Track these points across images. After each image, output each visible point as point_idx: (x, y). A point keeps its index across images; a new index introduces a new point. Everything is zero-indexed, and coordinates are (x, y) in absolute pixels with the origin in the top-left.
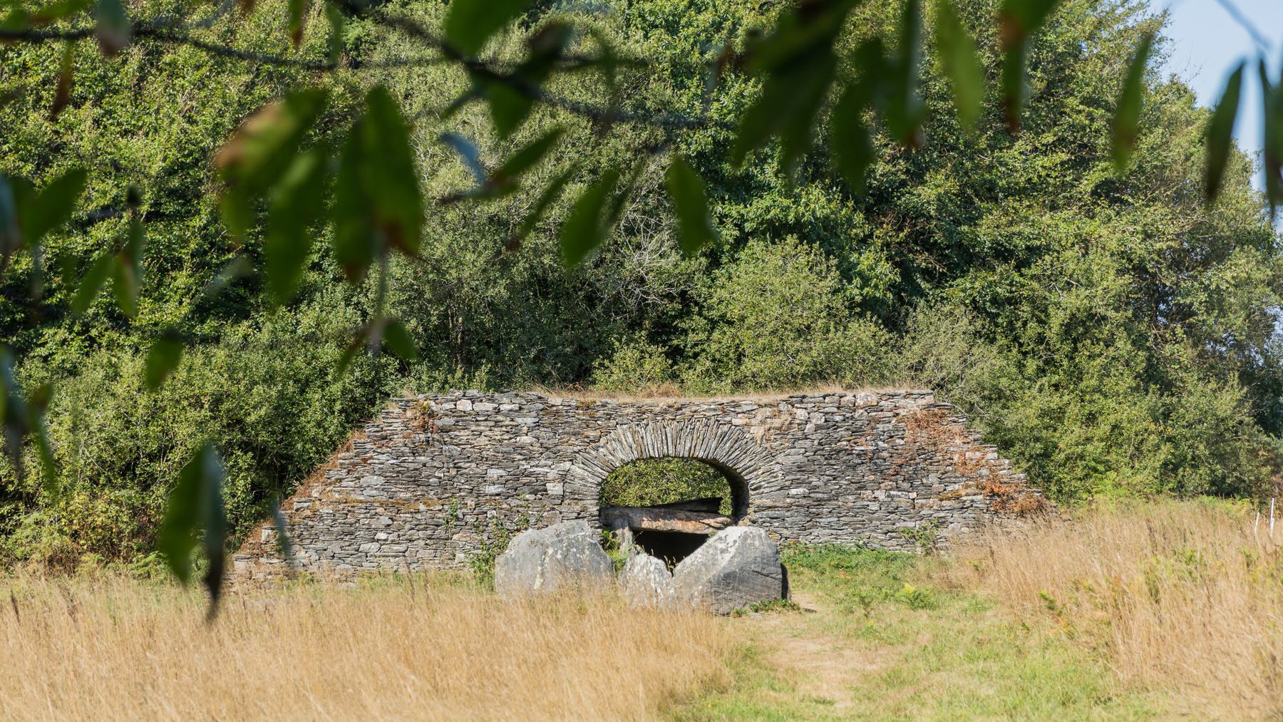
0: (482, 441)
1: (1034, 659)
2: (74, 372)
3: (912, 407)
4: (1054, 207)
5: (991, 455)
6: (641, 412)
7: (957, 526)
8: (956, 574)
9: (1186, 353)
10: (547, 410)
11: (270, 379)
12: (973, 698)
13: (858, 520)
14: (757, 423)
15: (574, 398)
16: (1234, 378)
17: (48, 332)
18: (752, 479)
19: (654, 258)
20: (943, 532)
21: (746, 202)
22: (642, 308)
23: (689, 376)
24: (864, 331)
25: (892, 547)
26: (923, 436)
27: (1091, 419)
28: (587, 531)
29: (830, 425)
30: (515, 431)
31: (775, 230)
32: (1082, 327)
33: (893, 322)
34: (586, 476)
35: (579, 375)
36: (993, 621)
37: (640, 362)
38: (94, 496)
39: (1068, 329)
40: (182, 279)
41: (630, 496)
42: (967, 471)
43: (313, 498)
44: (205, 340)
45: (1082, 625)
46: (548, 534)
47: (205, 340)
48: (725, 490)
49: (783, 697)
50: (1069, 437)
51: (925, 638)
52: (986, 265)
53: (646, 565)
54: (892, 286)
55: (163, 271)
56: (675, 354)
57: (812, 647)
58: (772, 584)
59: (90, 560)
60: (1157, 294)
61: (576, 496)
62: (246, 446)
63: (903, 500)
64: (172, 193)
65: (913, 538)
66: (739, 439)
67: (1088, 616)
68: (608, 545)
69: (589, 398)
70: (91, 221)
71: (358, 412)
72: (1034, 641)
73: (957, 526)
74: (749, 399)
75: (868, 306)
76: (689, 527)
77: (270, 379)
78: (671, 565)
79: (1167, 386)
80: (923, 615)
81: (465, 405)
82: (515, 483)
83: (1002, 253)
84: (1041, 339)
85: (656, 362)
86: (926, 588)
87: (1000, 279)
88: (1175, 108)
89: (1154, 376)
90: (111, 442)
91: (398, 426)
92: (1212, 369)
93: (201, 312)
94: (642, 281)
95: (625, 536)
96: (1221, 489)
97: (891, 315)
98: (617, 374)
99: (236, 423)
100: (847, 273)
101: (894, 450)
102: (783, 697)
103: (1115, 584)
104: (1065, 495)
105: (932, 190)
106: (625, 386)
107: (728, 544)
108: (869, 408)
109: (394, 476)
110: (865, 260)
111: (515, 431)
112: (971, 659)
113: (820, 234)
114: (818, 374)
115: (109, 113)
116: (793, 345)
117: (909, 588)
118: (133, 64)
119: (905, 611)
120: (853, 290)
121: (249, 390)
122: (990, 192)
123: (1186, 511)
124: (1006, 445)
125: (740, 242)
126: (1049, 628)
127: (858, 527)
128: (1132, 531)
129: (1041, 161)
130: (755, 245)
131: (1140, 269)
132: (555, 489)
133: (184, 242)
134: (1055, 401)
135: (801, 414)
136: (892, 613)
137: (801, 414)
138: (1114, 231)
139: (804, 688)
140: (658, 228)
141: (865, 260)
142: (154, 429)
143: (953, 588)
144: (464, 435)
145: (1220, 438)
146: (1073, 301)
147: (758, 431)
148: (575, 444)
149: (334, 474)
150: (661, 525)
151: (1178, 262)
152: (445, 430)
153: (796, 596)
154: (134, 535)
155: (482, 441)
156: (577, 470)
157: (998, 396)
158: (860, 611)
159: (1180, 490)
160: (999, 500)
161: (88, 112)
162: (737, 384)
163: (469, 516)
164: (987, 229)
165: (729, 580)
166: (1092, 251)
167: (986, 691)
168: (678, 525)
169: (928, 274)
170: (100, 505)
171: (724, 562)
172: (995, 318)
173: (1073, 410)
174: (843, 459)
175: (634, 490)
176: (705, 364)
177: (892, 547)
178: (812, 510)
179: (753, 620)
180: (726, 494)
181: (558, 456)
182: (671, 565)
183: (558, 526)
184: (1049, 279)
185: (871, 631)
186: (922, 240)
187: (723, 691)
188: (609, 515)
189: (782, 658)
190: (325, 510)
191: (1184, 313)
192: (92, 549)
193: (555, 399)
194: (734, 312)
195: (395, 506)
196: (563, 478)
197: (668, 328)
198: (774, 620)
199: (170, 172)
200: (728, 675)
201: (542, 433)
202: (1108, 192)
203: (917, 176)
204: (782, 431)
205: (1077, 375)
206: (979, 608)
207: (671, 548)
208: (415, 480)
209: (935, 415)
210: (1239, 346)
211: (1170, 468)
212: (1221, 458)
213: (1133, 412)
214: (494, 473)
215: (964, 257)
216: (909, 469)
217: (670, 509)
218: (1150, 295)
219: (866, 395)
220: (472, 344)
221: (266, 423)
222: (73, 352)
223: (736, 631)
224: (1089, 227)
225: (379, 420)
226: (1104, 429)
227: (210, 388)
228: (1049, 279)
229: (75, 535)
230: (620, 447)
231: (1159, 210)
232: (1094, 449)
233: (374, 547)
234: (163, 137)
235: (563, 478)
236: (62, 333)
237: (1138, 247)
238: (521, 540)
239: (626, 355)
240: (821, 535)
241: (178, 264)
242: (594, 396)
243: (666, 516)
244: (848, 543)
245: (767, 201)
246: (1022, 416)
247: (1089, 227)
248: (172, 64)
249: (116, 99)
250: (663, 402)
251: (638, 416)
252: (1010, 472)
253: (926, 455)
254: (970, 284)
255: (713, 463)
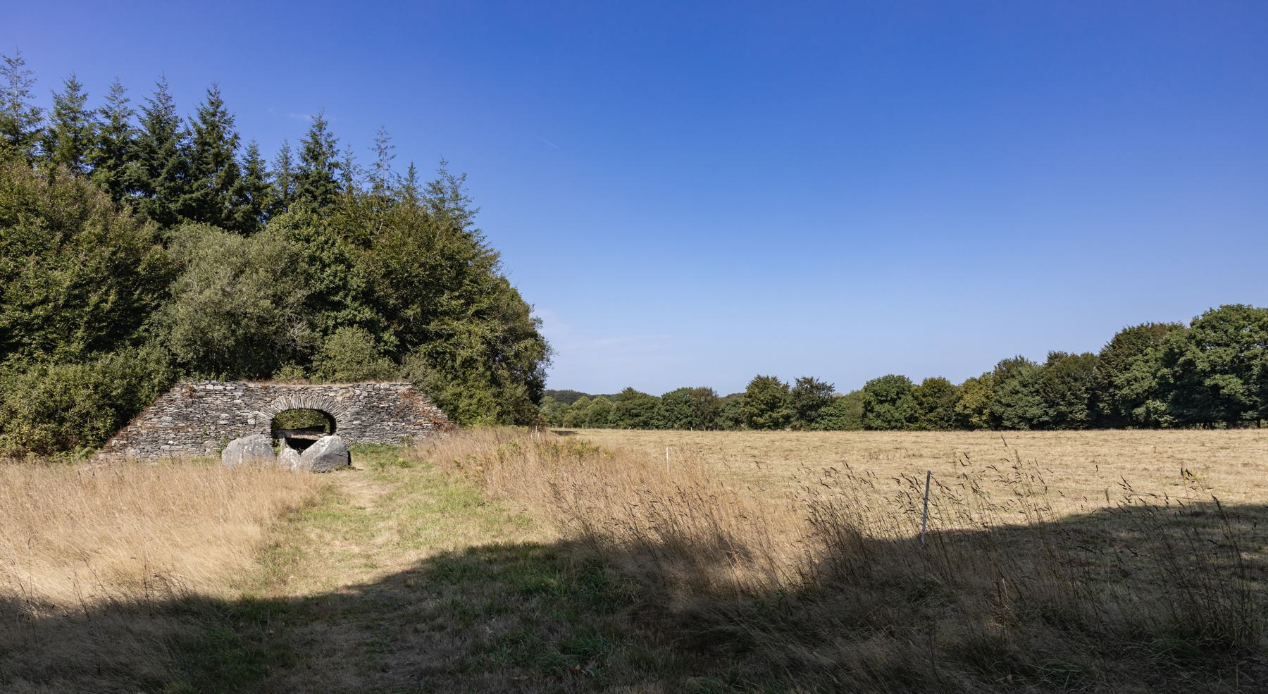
0: (218, 402)
1: (452, 487)
2: (24, 372)
3: (403, 389)
4: (458, 320)
5: (434, 408)
6: (290, 390)
7: (421, 435)
8: (420, 454)
9: (506, 373)
10: (248, 389)
11: (123, 377)
12: (427, 505)
13: (382, 434)
14: (337, 395)
15: (259, 385)
16: (522, 383)
17: (11, 355)
18: (337, 418)
19: (299, 332)
20: (416, 438)
21: (339, 311)
22: (294, 350)
23: (313, 378)
24: (384, 363)
25: (395, 444)
26: (407, 401)
27: (471, 397)
28: (266, 440)
29: (369, 396)
30: (233, 398)
31: (351, 323)
32: (469, 363)
33: (397, 361)
34: (266, 417)
35: (268, 377)
36: (435, 471)
37: (292, 373)
38: (34, 427)
39: (463, 364)
40: (80, 333)
41: (288, 425)
42: (425, 415)
43: (139, 425)
44: (91, 360)
45: (471, 473)
46: (246, 440)
47: (91, 360)
48: (325, 422)
49: (342, 507)
50: (463, 404)
51: (407, 480)
52: (432, 339)
53: (288, 452)
54: (396, 346)
55: (70, 330)
56: (307, 370)
57: (359, 485)
58: (344, 459)
59: (31, 454)
60: (495, 352)
61: (261, 425)
62: (111, 406)
63: (400, 425)
64: (76, 297)
65: (403, 440)
66: (332, 402)
67: (474, 468)
68: (275, 445)
69: (267, 385)
70: (34, 305)
71: (164, 389)
72: (451, 480)
73: (421, 435)
74: (336, 386)
75: (387, 353)
76: (311, 437)
77: (123, 377)
78: (300, 453)
79: (499, 385)
80: (406, 470)
81: (210, 387)
82: (233, 420)
83: (439, 335)
84: (453, 367)
85: (299, 372)
86: (407, 459)
87: (439, 345)
88: (504, 286)
89: (495, 381)
90: (43, 403)
91: (178, 395)
92: (515, 380)
93: (89, 348)
94: (294, 341)
95: (282, 441)
96: (518, 423)
97: (396, 357)
98: (283, 377)
99: (106, 395)
100: (378, 340)
101: (396, 407)
102: (342, 507)
103: (485, 455)
104: (463, 425)
105: (411, 312)
106: (287, 381)
107: (324, 443)
108: (386, 390)
109: (177, 417)
110: (386, 336)
111: (233, 398)
112: (426, 487)
113: (370, 326)
114: (365, 378)
115: (44, 260)
116: (355, 366)
117: (401, 459)
118: (57, 239)
119: (399, 469)
120: (382, 347)
121: (112, 382)
122: (435, 314)
123: (508, 429)
124: (440, 407)
125: (335, 327)
126: (458, 474)
127: (381, 437)
128: (490, 435)
129: (453, 302)
130: (340, 329)
131: (489, 343)
132: (251, 422)
133: (81, 317)
134: (458, 390)
135: (358, 392)
136: (394, 470)
137: (358, 392)
138: (481, 329)
139: (353, 502)
140: (301, 320)
141: (386, 336)
142: (66, 398)
143: (419, 460)
144: (210, 399)
145: (518, 403)
146: (464, 354)
147: (340, 399)
148: (261, 403)
149: (148, 416)
150: (299, 437)
151: (505, 341)
152: (201, 397)
153: (355, 464)
154: (54, 444)
155: (218, 402)
156: (261, 414)
157: (437, 388)
158: (380, 469)
159: (504, 423)
160: (438, 426)
161: (32, 259)
162: (334, 382)
163: (209, 432)
164: (433, 326)
165: (326, 458)
166: (472, 336)
167: (432, 501)
168: (306, 437)
169: (412, 343)
170: (37, 431)
171: (323, 451)
172: (435, 359)
173: (465, 393)
174: (373, 410)
175: (290, 423)
176: (320, 374)
177: (395, 444)
178: (362, 430)
179: (335, 474)
180: (327, 426)
181: (253, 409)
182: (300, 453)
183: (252, 437)
184: (456, 345)
185: (384, 478)
186: (408, 330)
187: (314, 505)
188: (277, 430)
189: (345, 490)
190: (144, 432)
191: (505, 359)
192: (33, 450)
193: (251, 385)
194: (332, 354)
195: (177, 429)
196: (255, 417)
197: (305, 360)
198: (344, 473)
199: (75, 286)
200: (318, 498)
201: (246, 399)
202: (479, 314)
203: (406, 306)
204: (350, 398)
205: (465, 381)
206: (429, 467)
207: (300, 445)
208: (187, 418)
209: (411, 393)
210: (525, 373)
211: (500, 415)
212: (518, 411)
213: (487, 395)
214: (224, 415)
215: (425, 337)
216: (402, 414)
217: (302, 431)
218: (492, 351)
219: (385, 385)
220: (212, 361)
221: (121, 396)
222: (24, 363)
223: (323, 479)
224: (472, 327)
225: (171, 394)
226: (475, 401)
227: (93, 380)
228: (456, 345)
229: (24, 445)
230: (280, 404)
231: (496, 322)
232: (473, 407)
233: (167, 447)
234: (70, 272)
235: (255, 417)
236: (17, 356)
237: (489, 335)
238: (232, 445)
239: (287, 369)
240: (366, 440)
241: (78, 327)
242: (269, 384)
243: (294, 432)
244: (377, 442)
245: (348, 311)
246: (446, 395)
247: (472, 327)
248: (77, 240)
249: (49, 253)
250: (299, 387)
251: (289, 393)
252: (441, 415)
253: (409, 408)
254: (423, 348)
255: (320, 411)
